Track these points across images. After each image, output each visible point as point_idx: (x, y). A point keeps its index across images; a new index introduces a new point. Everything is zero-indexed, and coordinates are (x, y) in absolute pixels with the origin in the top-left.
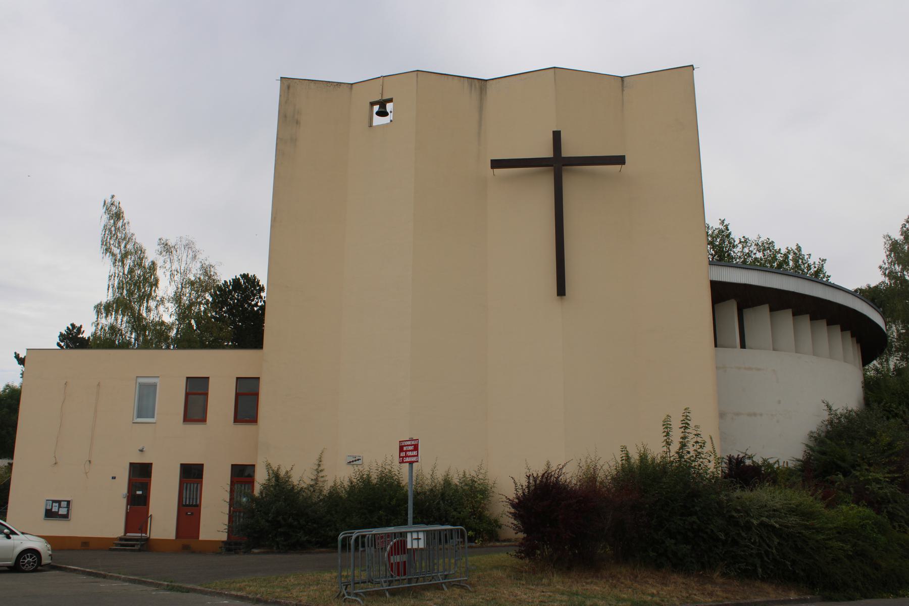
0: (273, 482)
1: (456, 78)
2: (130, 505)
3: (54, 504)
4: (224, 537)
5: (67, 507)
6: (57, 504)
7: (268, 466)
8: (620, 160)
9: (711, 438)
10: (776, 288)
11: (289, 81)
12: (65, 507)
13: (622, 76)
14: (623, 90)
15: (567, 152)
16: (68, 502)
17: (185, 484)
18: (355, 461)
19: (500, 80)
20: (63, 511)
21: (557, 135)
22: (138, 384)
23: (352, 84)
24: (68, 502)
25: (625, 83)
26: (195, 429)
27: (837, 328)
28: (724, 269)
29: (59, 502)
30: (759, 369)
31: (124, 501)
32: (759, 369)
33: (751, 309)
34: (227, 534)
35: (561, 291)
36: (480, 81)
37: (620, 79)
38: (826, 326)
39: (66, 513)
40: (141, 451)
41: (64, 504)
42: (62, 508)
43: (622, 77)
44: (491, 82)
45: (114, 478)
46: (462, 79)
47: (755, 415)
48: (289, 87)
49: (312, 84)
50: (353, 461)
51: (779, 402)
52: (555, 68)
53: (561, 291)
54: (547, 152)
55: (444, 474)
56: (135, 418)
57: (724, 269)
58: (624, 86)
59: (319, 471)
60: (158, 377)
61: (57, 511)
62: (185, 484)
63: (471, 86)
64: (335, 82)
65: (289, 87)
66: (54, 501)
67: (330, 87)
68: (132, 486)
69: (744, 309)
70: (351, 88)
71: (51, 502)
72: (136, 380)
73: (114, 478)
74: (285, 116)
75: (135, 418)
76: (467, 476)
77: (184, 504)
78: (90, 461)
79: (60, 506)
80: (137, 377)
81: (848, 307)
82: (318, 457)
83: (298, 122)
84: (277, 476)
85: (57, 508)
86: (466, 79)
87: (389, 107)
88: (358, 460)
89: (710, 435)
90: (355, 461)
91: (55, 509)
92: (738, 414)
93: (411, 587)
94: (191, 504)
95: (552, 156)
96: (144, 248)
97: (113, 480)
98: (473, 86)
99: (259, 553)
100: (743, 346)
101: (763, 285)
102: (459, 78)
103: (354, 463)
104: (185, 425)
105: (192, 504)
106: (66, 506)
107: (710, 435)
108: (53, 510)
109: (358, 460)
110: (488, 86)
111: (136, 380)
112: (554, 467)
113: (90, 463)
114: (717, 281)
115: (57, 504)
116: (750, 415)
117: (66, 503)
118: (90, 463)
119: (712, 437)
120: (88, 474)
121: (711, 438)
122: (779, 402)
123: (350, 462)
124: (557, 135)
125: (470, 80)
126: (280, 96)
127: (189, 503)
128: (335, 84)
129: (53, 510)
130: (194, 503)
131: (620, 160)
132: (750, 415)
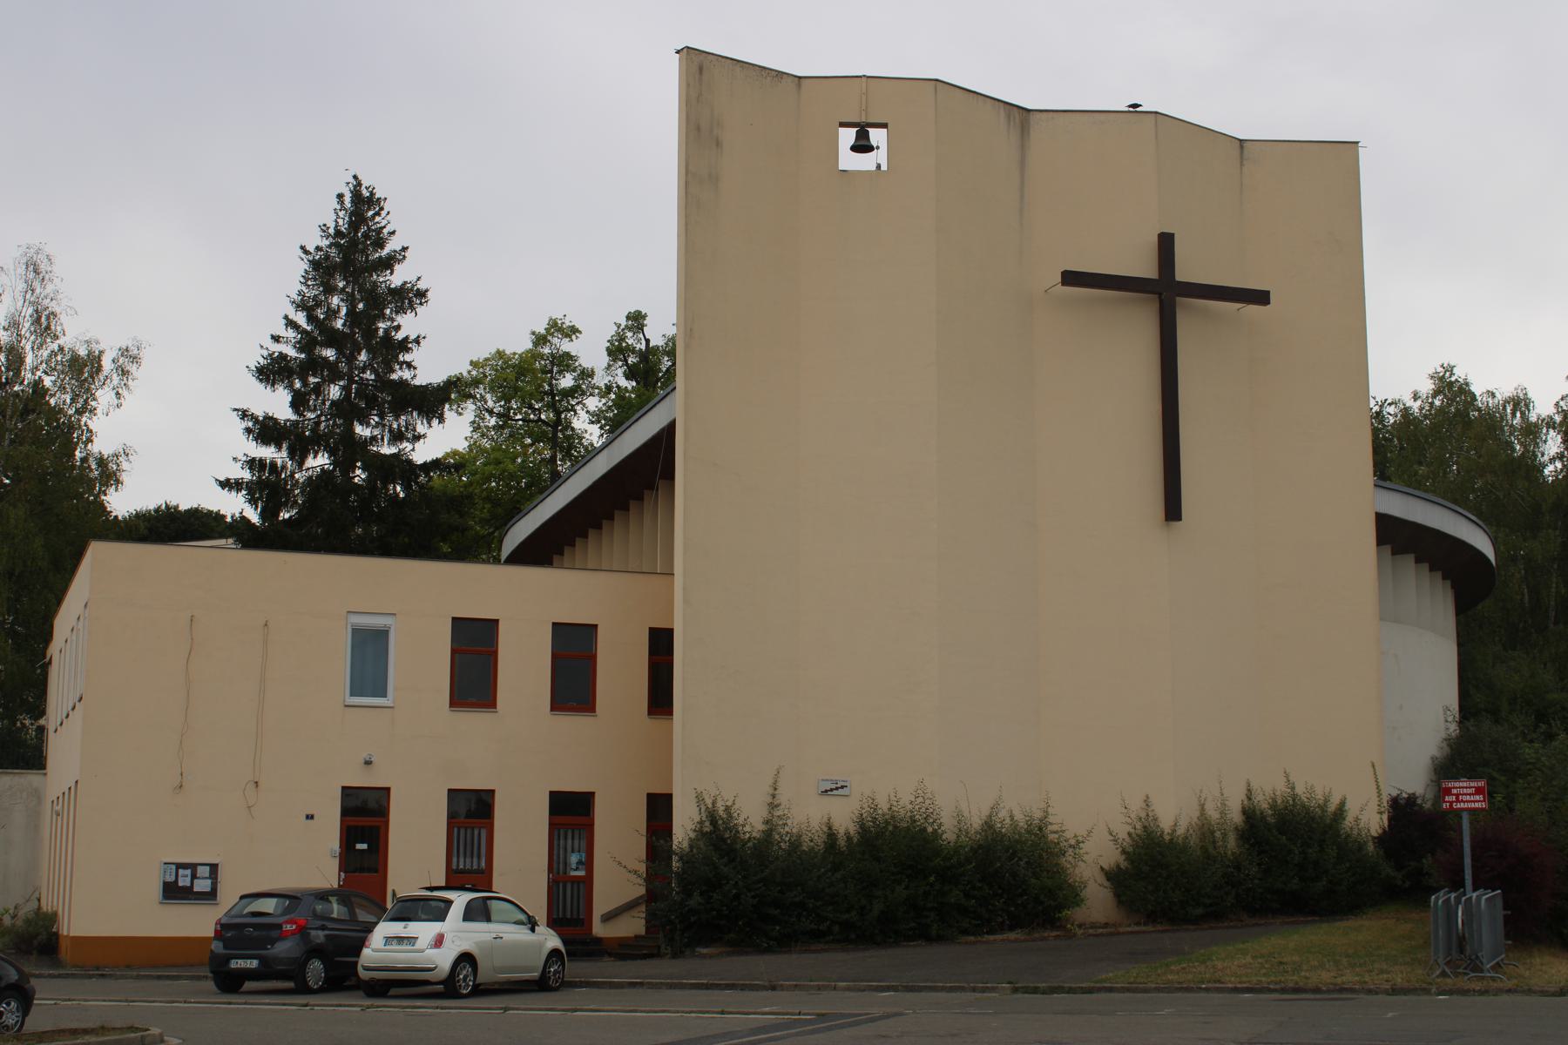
0: (708, 828)
1: (989, 100)
2: (345, 872)
3: (181, 872)
4: (213, 935)
5: (210, 878)
6: (188, 872)
7: (700, 799)
8: (1261, 298)
12: (206, 878)
14: (1242, 164)
15: (1184, 273)
16: (214, 868)
17: (456, 830)
18: (837, 789)
19: (1055, 114)
20: (202, 885)
21: (1166, 243)
23: (800, 78)
24: (214, 868)
25: (1246, 152)
26: (473, 721)
27: (1409, 559)
29: (193, 867)
31: (336, 863)
34: (643, 922)
35: (1173, 510)
37: (1239, 142)
38: (1390, 557)
39: (209, 889)
40: (368, 763)
41: (204, 871)
42: (199, 878)
43: (1241, 140)
44: (1038, 115)
45: (310, 817)
46: (997, 103)
50: (832, 790)
52: (1156, 113)
53: (1173, 510)
54: (1145, 267)
55: (985, 812)
59: (773, 806)
60: (395, 614)
61: (189, 885)
62: (456, 830)
63: (1009, 118)
64: (773, 70)
65: (701, 69)
66: (179, 866)
67: (766, 78)
68: (349, 835)
70: (799, 86)
71: (174, 867)
73: (310, 817)
74: (698, 129)
76: (1003, 814)
77: (454, 867)
78: (256, 783)
79: (194, 876)
80: (348, 612)
81: (1446, 534)
82: (771, 781)
83: (718, 144)
84: (712, 817)
85: (189, 879)
86: (1002, 104)
87: (877, 136)
88: (842, 787)
90: (837, 789)
91: (184, 881)
93: (1494, 959)
95: (1157, 278)
96: (457, 373)
97: (309, 821)
98: (1012, 119)
99: (710, 956)
102: (993, 101)
103: (835, 792)
104: (452, 713)
105: (458, 869)
106: (207, 875)
108: (180, 884)
109: (842, 787)
113: (257, 786)
115: (188, 872)
117: (208, 868)
118: (257, 786)
120: (252, 809)
123: (826, 791)
124: (1166, 243)
125: (1008, 107)
127: (465, 866)
129: (180, 884)
130: (475, 867)
131: (1261, 298)
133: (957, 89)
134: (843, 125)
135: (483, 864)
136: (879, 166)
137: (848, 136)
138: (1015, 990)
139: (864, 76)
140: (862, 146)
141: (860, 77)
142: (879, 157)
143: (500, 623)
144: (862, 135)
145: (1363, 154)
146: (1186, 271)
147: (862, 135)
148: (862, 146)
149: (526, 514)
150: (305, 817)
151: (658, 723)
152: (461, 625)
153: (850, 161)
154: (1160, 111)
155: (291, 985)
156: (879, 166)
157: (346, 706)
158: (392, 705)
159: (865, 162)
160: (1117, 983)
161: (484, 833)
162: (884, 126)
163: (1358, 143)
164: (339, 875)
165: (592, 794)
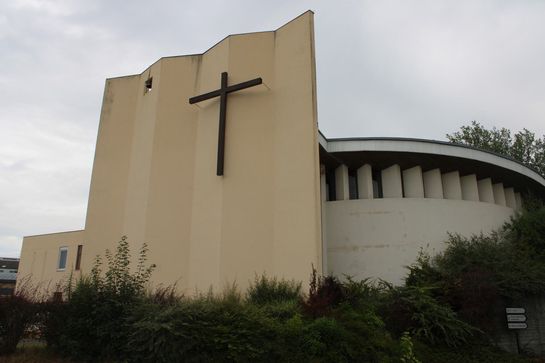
8: (259, 81)
9: (312, 265)
10: (443, 154)
11: (110, 80)
13: (275, 30)
14: (275, 39)
22: (60, 250)
28: (452, 148)
30: (387, 213)
32: (387, 213)
33: (386, 169)
36: (199, 55)
46: (188, 56)
47: (382, 246)
48: (109, 83)
49: (121, 79)
51: (405, 236)
52: (230, 36)
53: (221, 171)
56: (58, 269)
57: (331, 144)
58: (276, 36)
65: (109, 83)
67: (130, 78)
69: (382, 170)
72: (60, 248)
74: (106, 99)
75: (58, 269)
89: (312, 263)
92: (368, 247)
94: (523, 319)
98: (194, 59)
100: (404, 197)
101: (380, 150)
107: (312, 263)
110: (203, 57)
111: (60, 248)
112: (165, 287)
114: (342, 152)
116: (377, 247)
119: (313, 264)
121: (312, 265)
122: (405, 236)
126: (105, 89)
128: (132, 76)
131: (259, 81)
132: (377, 247)
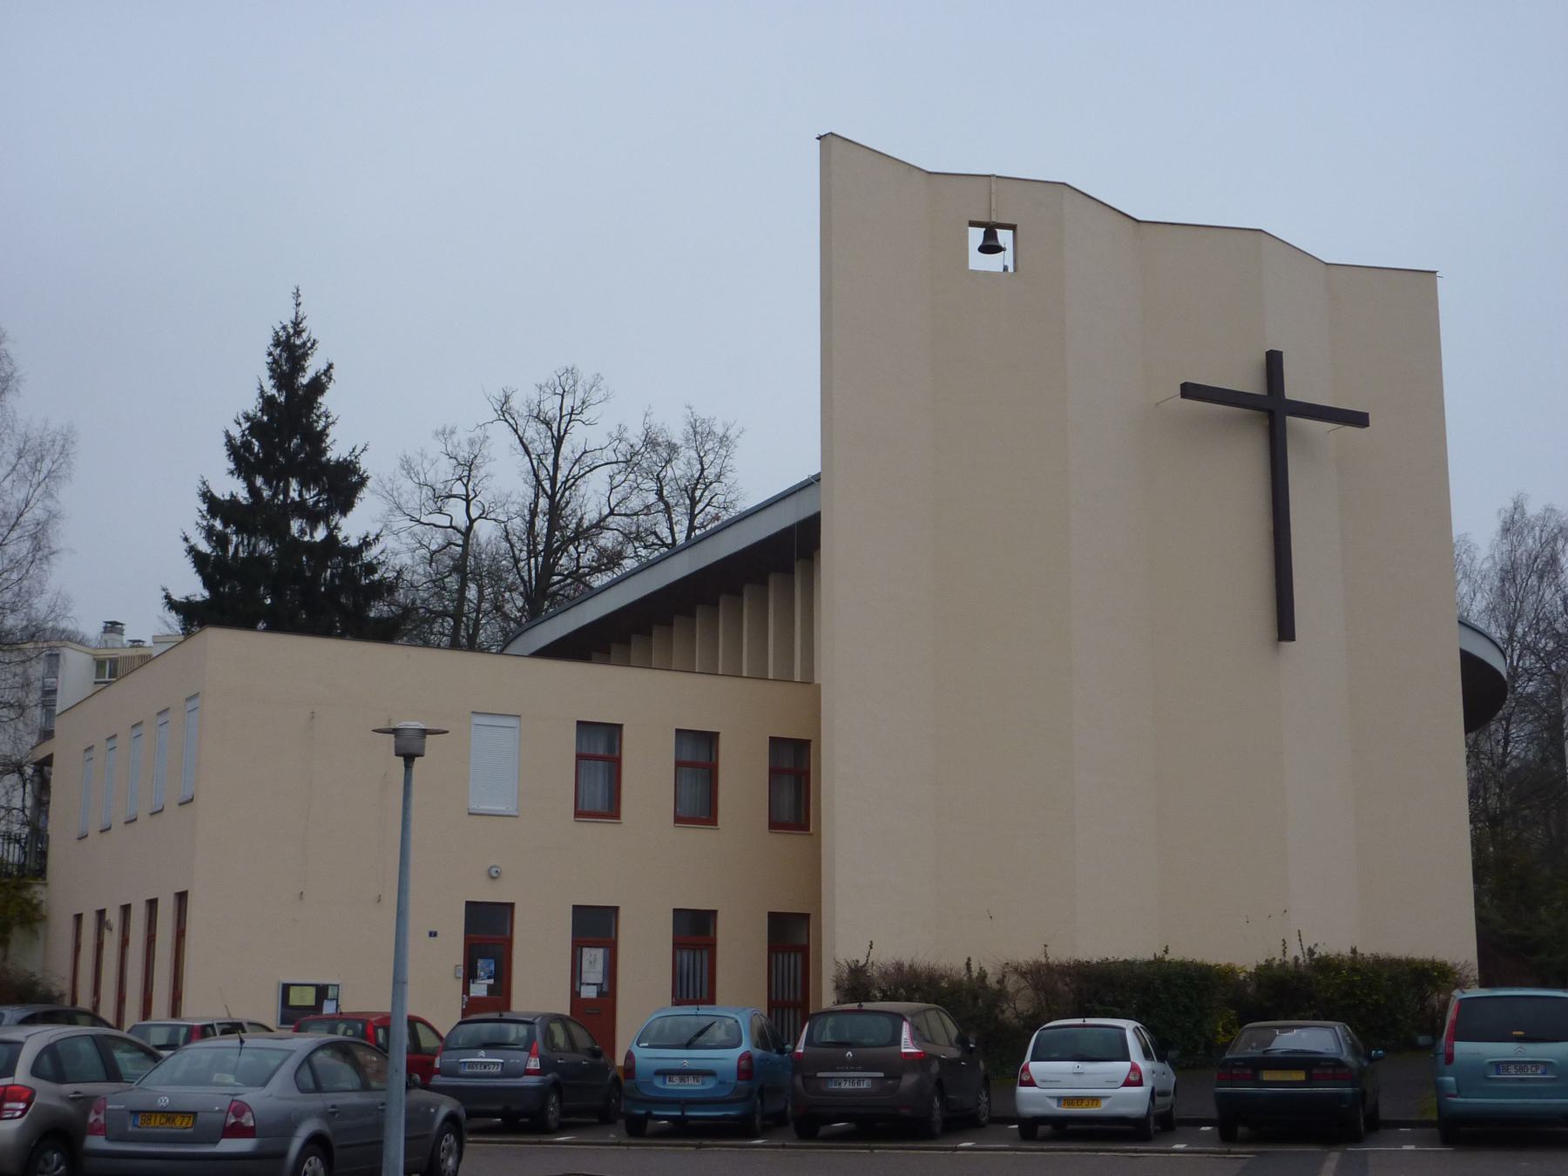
21: (1274, 361)
54: (1250, 381)
73: (433, 934)
80: (473, 712)
87: (1004, 237)
133: (970, 178)
134: (973, 224)
135: (799, 997)
136: (1006, 268)
137: (976, 236)
138: (195, 1114)
139: (994, 176)
140: (990, 247)
141: (990, 176)
142: (1004, 259)
143: (625, 729)
144: (990, 233)
145: (1441, 284)
146: (1294, 390)
147: (990, 233)
148: (990, 247)
149: (579, 603)
150: (428, 934)
151: (788, 842)
152: (585, 728)
153: (981, 262)
154: (1264, 229)
155: (1070, 1127)
156: (1006, 268)
157: (470, 814)
158: (516, 814)
159: (993, 263)
160: (401, 1101)
161: (705, 955)
162: (1013, 227)
163: (1435, 272)
164: (463, 998)
165: (714, 913)
